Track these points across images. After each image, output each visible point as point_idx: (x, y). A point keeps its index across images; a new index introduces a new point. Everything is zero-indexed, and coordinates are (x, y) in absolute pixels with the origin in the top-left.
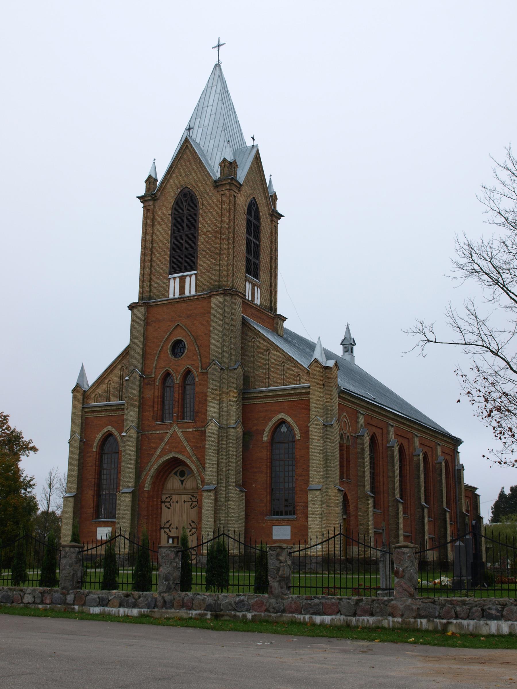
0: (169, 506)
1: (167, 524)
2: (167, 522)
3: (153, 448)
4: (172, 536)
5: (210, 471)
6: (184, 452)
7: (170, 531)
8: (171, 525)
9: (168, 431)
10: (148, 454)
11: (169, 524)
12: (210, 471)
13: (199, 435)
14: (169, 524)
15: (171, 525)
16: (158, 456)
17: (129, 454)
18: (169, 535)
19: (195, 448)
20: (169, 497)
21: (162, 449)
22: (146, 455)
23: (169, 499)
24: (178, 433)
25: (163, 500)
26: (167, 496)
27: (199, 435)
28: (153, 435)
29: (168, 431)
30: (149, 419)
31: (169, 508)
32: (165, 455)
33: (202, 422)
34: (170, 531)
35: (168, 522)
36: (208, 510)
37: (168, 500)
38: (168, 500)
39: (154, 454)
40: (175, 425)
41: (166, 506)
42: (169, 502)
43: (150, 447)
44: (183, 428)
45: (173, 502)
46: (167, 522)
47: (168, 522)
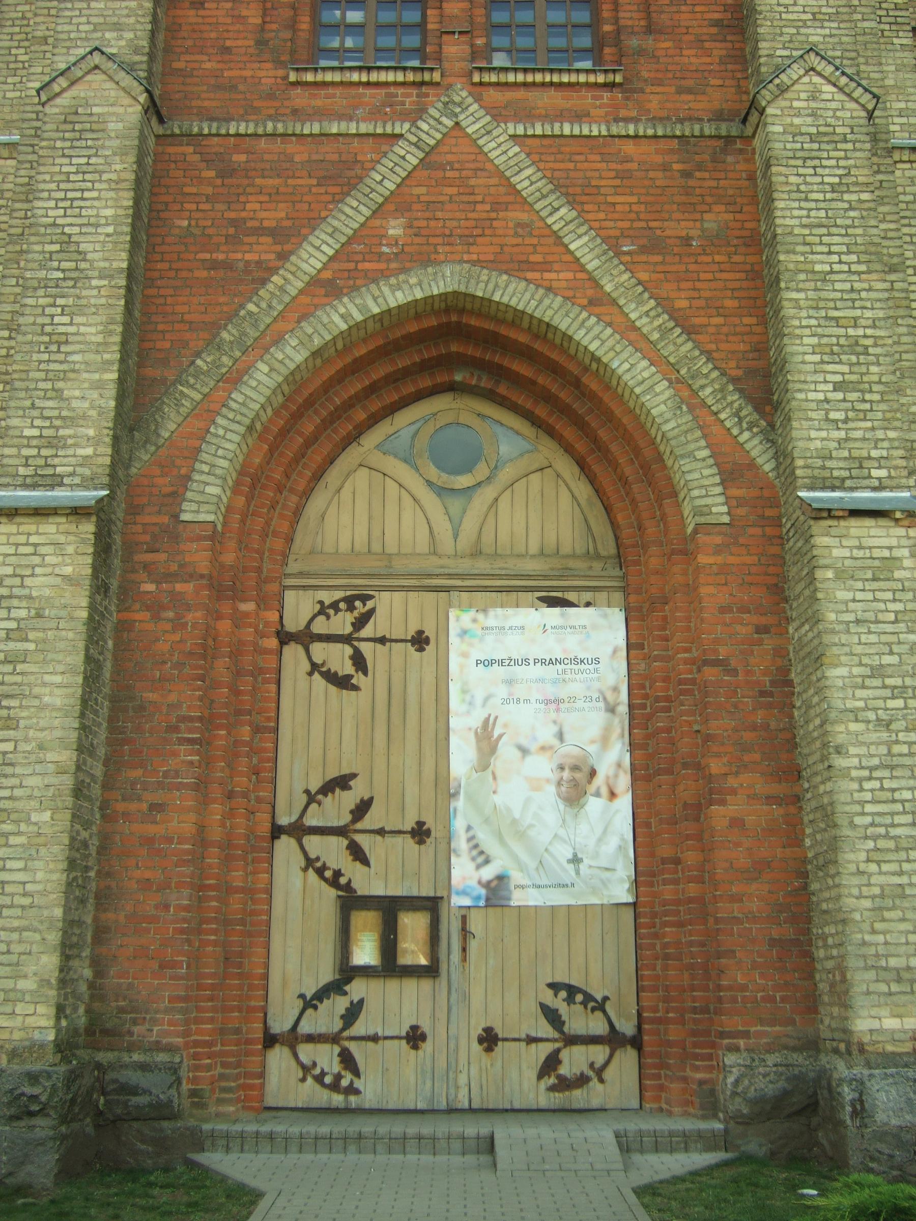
0: (348, 668)
1: (328, 801)
2: (328, 788)
3: (260, 231)
4: (378, 889)
5: (837, 387)
6: (545, 266)
7: (358, 854)
8: (362, 808)
9: (402, 128)
10: (214, 265)
11: (348, 799)
12: (837, 387)
13: (665, 168)
14: (348, 799)
15: (362, 808)
16: (315, 282)
17: (67, 240)
18: (348, 887)
19: (643, 250)
20: (349, 602)
21: (350, 240)
22: (204, 274)
23: (349, 618)
24: (488, 145)
25: (293, 624)
26: (328, 597)
27: (665, 168)
28: (263, 143)
29: (402, 128)
30: (227, 50)
31: (343, 682)
32: (374, 278)
33: (680, 91)
34: (358, 854)
35: (342, 782)
36: (878, 671)
37: (342, 623)
38: (342, 623)
39: (274, 271)
40: (461, 93)
41: (315, 667)
42: (346, 639)
43: (234, 223)
44: (527, 115)
45: (382, 640)
46: (328, 788)
47: (342, 782)
